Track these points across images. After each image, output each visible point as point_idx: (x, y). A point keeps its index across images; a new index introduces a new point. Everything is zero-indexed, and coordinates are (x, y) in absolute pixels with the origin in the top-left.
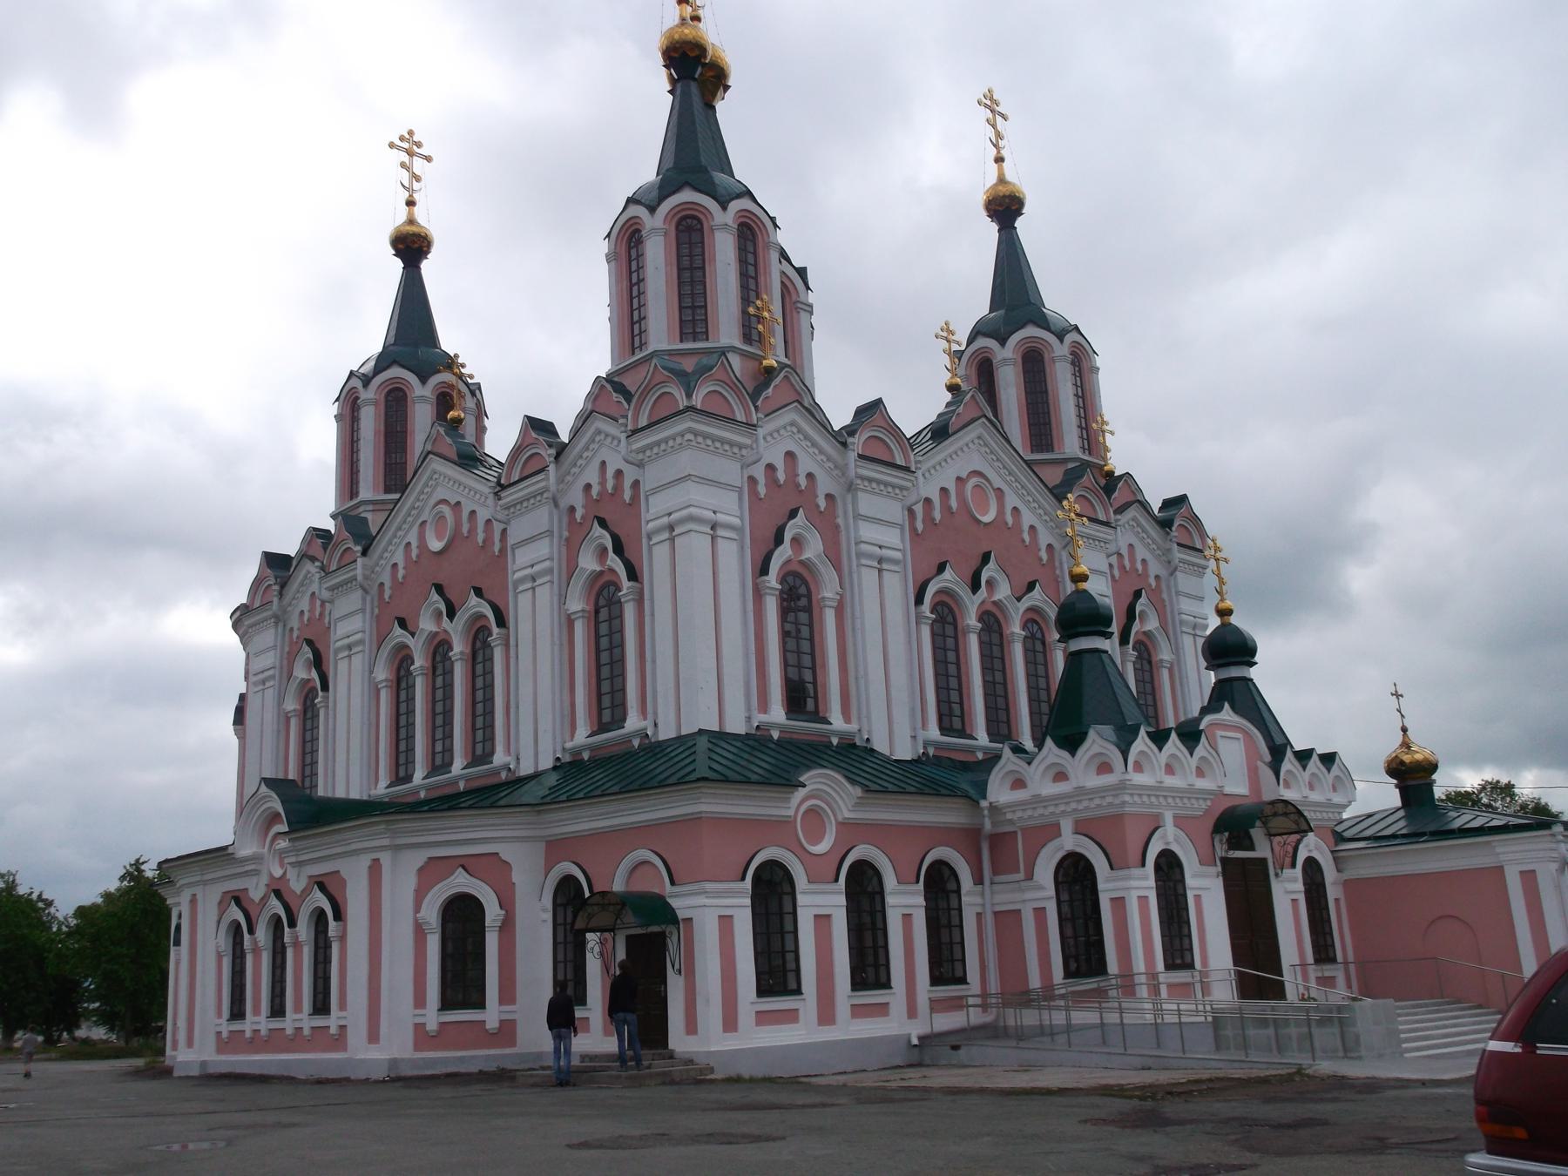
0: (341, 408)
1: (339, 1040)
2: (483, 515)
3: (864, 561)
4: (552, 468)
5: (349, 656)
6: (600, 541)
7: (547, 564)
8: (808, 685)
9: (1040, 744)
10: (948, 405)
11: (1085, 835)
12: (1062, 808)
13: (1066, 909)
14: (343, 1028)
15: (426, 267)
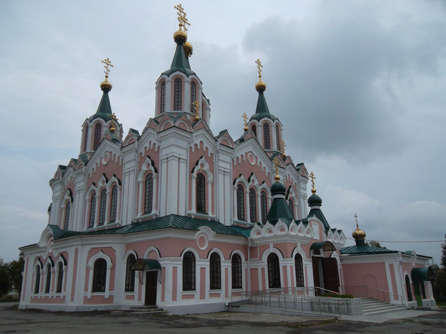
0: (84, 128)
1: (63, 300)
2: (117, 155)
3: (220, 172)
4: (136, 142)
5: (79, 193)
6: (148, 162)
7: (133, 168)
8: (203, 204)
9: (264, 223)
10: (244, 134)
11: (278, 249)
12: (270, 240)
13: (270, 268)
14: (64, 296)
15: (110, 93)
